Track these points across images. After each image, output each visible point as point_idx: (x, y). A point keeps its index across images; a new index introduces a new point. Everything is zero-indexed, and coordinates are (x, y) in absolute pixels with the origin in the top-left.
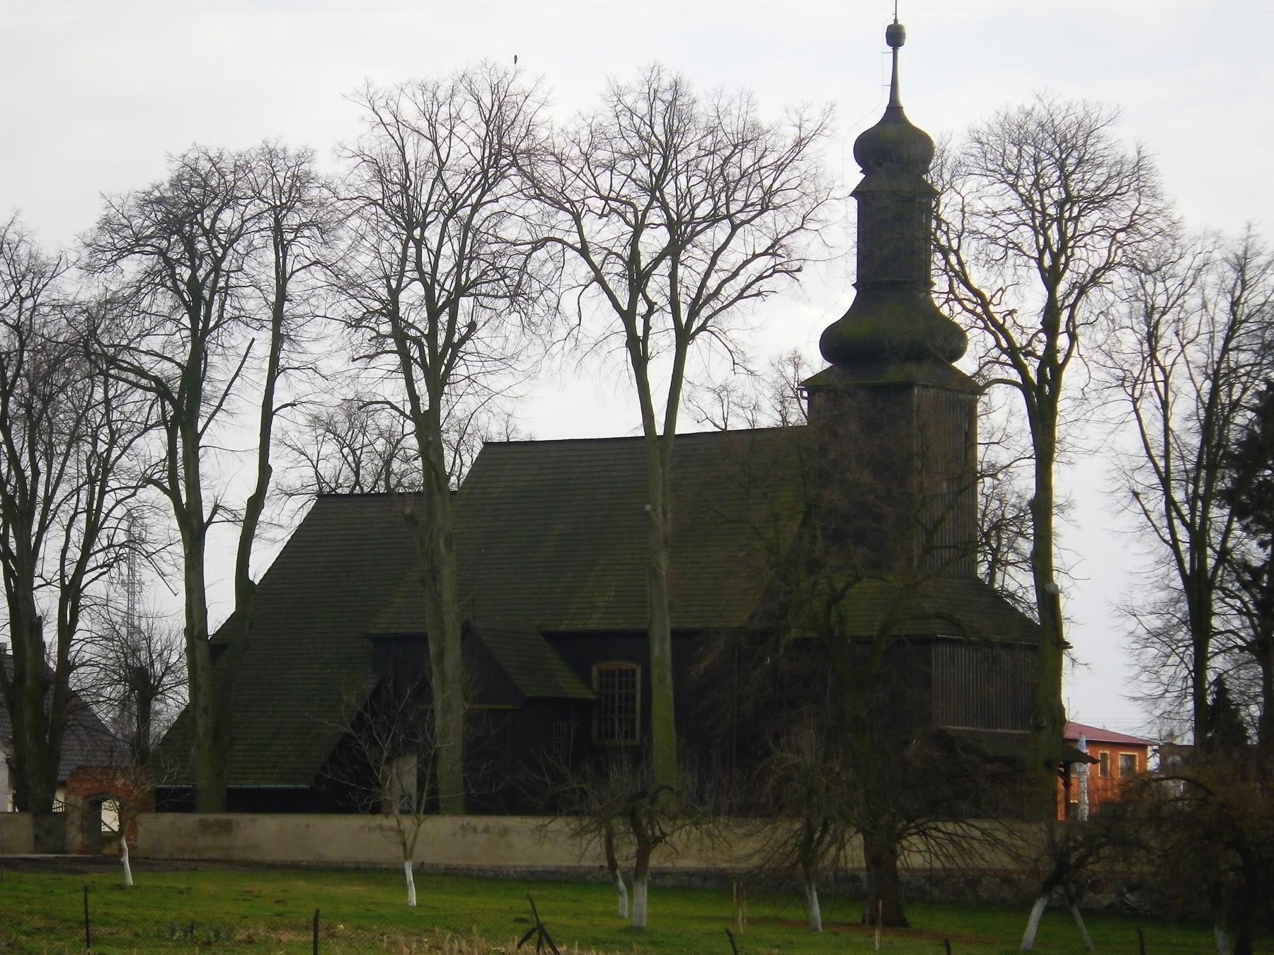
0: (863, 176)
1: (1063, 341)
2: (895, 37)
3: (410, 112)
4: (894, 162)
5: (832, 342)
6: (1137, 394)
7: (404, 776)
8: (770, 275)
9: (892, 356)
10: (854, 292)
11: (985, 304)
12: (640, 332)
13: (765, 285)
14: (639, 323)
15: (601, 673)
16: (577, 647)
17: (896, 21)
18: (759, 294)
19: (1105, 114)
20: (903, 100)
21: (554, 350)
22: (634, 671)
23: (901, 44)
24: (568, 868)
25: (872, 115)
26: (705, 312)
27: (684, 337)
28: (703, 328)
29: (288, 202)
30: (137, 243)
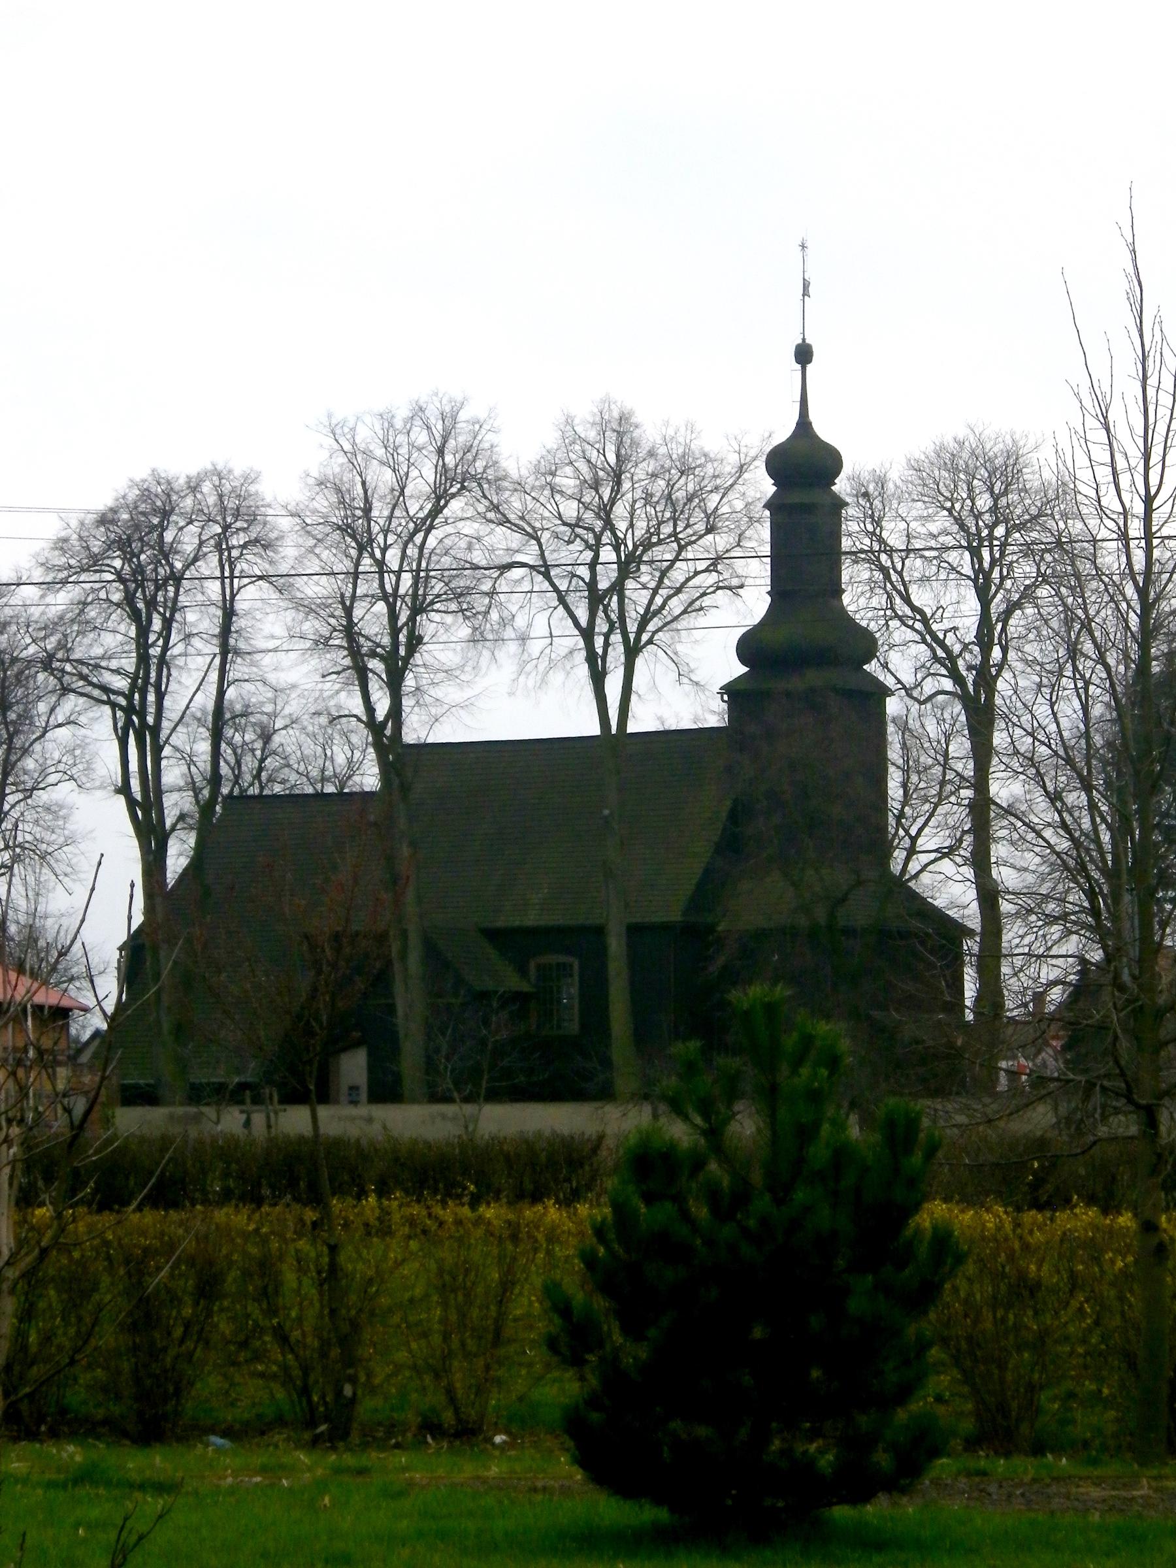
0: (775, 488)
1: (996, 653)
2: (804, 355)
3: (364, 436)
4: (804, 471)
5: (748, 648)
6: (1054, 699)
7: (354, 1067)
8: (714, 592)
9: (805, 662)
10: (769, 599)
11: (925, 621)
12: (600, 651)
13: (706, 601)
14: (599, 642)
15: (539, 967)
16: (513, 942)
17: (804, 340)
18: (701, 609)
19: (1031, 443)
20: (813, 416)
21: (529, 667)
22: (571, 966)
23: (810, 361)
24: (415, 1142)
25: (784, 431)
26: (651, 627)
27: (632, 652)
28: (650, 642)
29: (235, 521)
30: (94, 563)
